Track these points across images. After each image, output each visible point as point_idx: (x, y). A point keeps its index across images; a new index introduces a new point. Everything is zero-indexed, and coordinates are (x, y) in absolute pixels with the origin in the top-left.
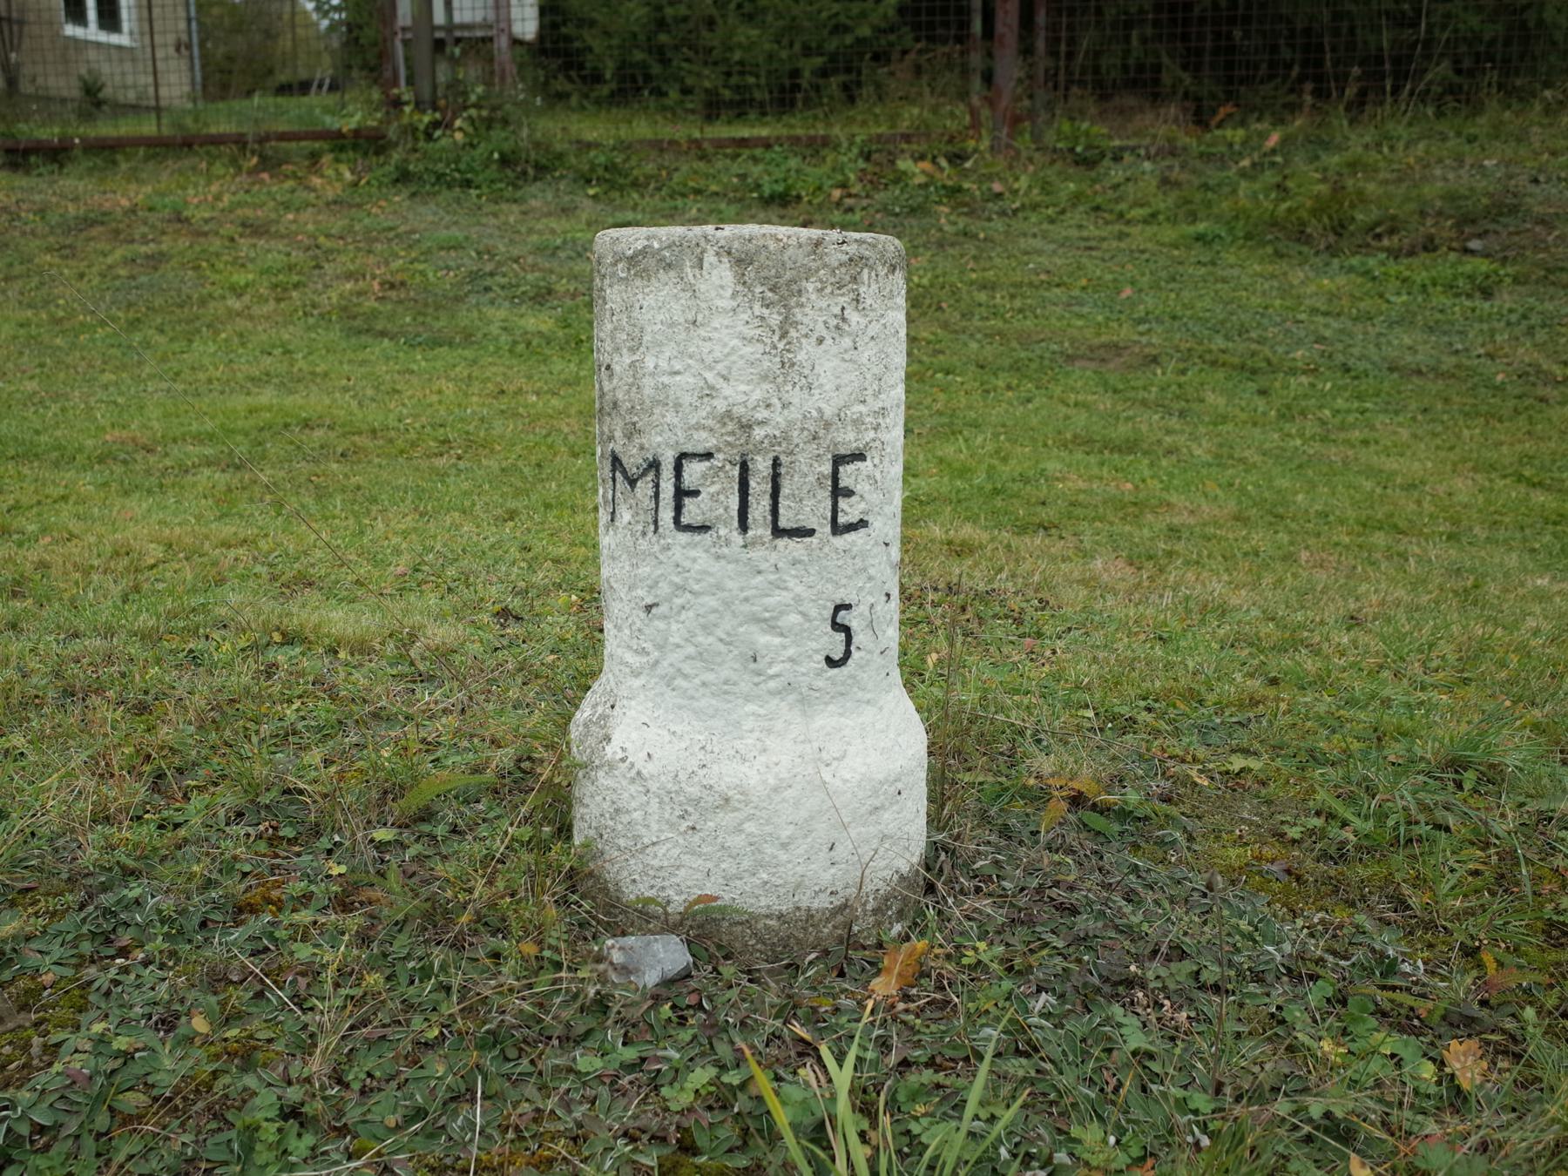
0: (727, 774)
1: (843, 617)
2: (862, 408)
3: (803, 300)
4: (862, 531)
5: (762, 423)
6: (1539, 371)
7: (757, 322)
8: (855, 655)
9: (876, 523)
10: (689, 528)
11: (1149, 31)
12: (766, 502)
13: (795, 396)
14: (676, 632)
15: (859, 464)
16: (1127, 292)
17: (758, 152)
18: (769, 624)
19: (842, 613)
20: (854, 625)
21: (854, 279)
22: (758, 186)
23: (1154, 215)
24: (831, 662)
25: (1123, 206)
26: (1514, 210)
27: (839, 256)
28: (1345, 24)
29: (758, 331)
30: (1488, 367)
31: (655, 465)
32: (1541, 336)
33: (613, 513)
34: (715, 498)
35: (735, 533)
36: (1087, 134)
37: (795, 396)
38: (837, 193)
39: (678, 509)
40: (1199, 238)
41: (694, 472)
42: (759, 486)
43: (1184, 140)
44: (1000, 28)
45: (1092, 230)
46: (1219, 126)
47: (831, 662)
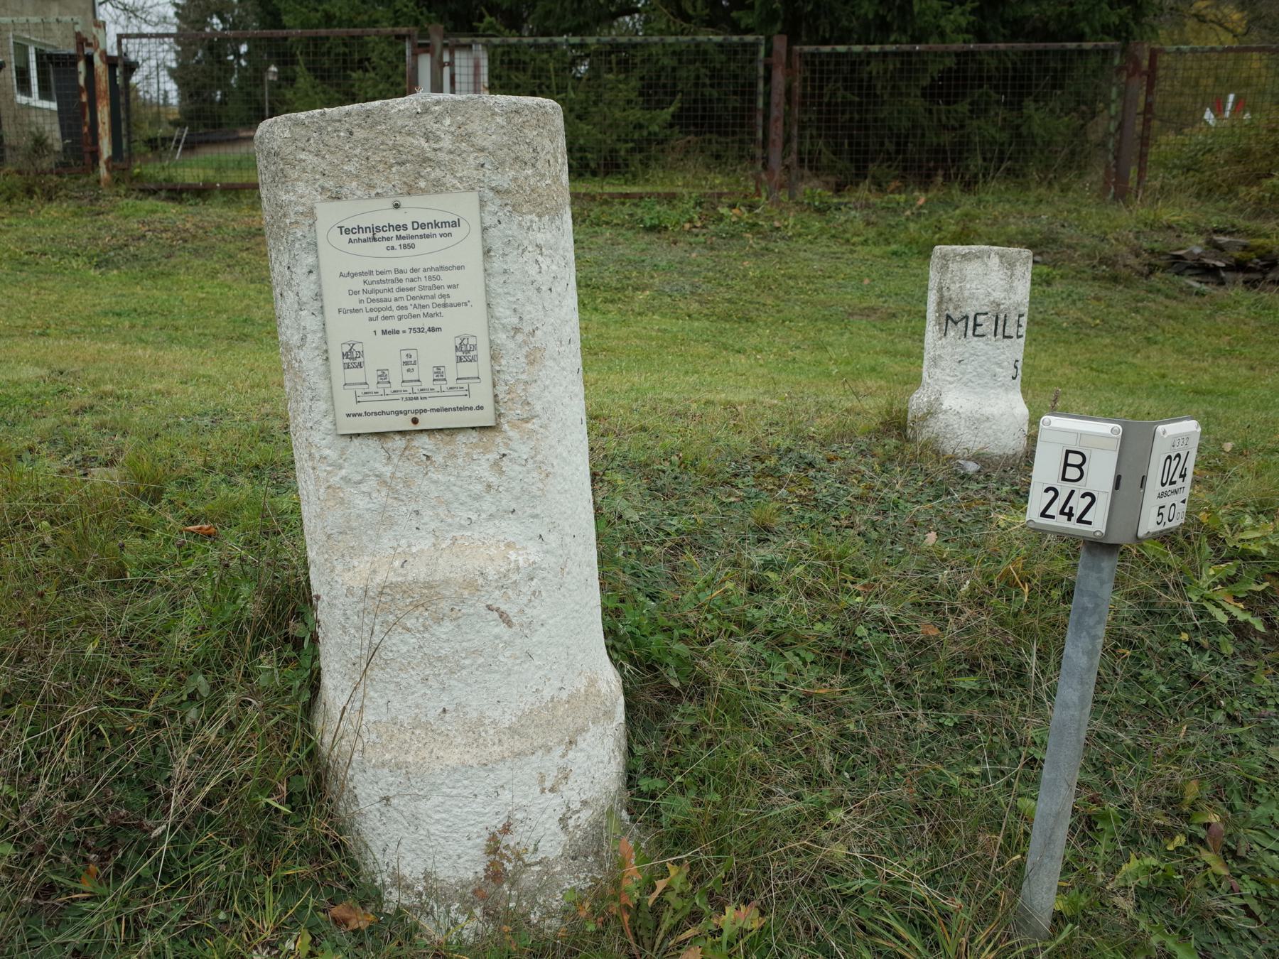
0: (987, 410)
6: (1082, 322)
11: (815, 132)
13: (1012, 296)
14: (970, 368)
16: (867, 281)
17: (636, 201)
18: (999, 365)
22: (642, 221)
23: (866, 241)
25: (848, 236)
26: (1055, 241)
28: (919, 132)
30: (1058, 320)
31: (966, 317)
32: (1079, 304)
34: (987, 325)
36: (820, 195)
37: (1012, 296)
38: (687, 226)
40: (895, 253)
41: (980, 319)
42: (1001, 323)
43: (872, 199)
44: (773, 136)
45: (835, 248)
46: (892, 192)
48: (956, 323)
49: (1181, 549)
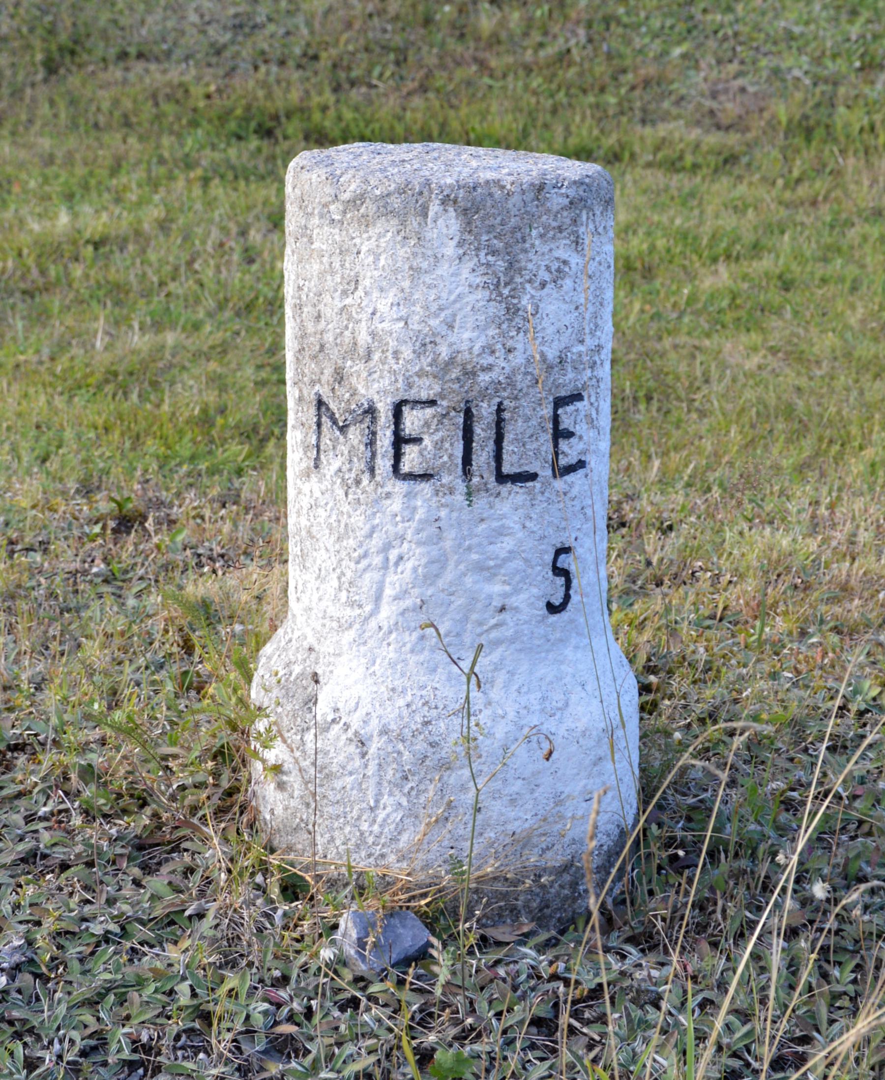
1: (564, 561)
2: (582, 348)
3: (527, 245)
4: (581, 472)
5: (489, 368)
7: (483, 269)
8: (575, 598)
9: (592, 461)
10: (411, 476)
12: (491, 446)
15: (579, 405)
19: (562, 557)
20: (573, 569)
21: (575, 221)
24: (552, 609)
27: (560, 200)
29: (485, 279)
33: (317, 459)
35: (459, 481)
39: (398, 456)
42: (482, 432)
47: (552, 609)
48: (343, 429)
49: (702, 909)
